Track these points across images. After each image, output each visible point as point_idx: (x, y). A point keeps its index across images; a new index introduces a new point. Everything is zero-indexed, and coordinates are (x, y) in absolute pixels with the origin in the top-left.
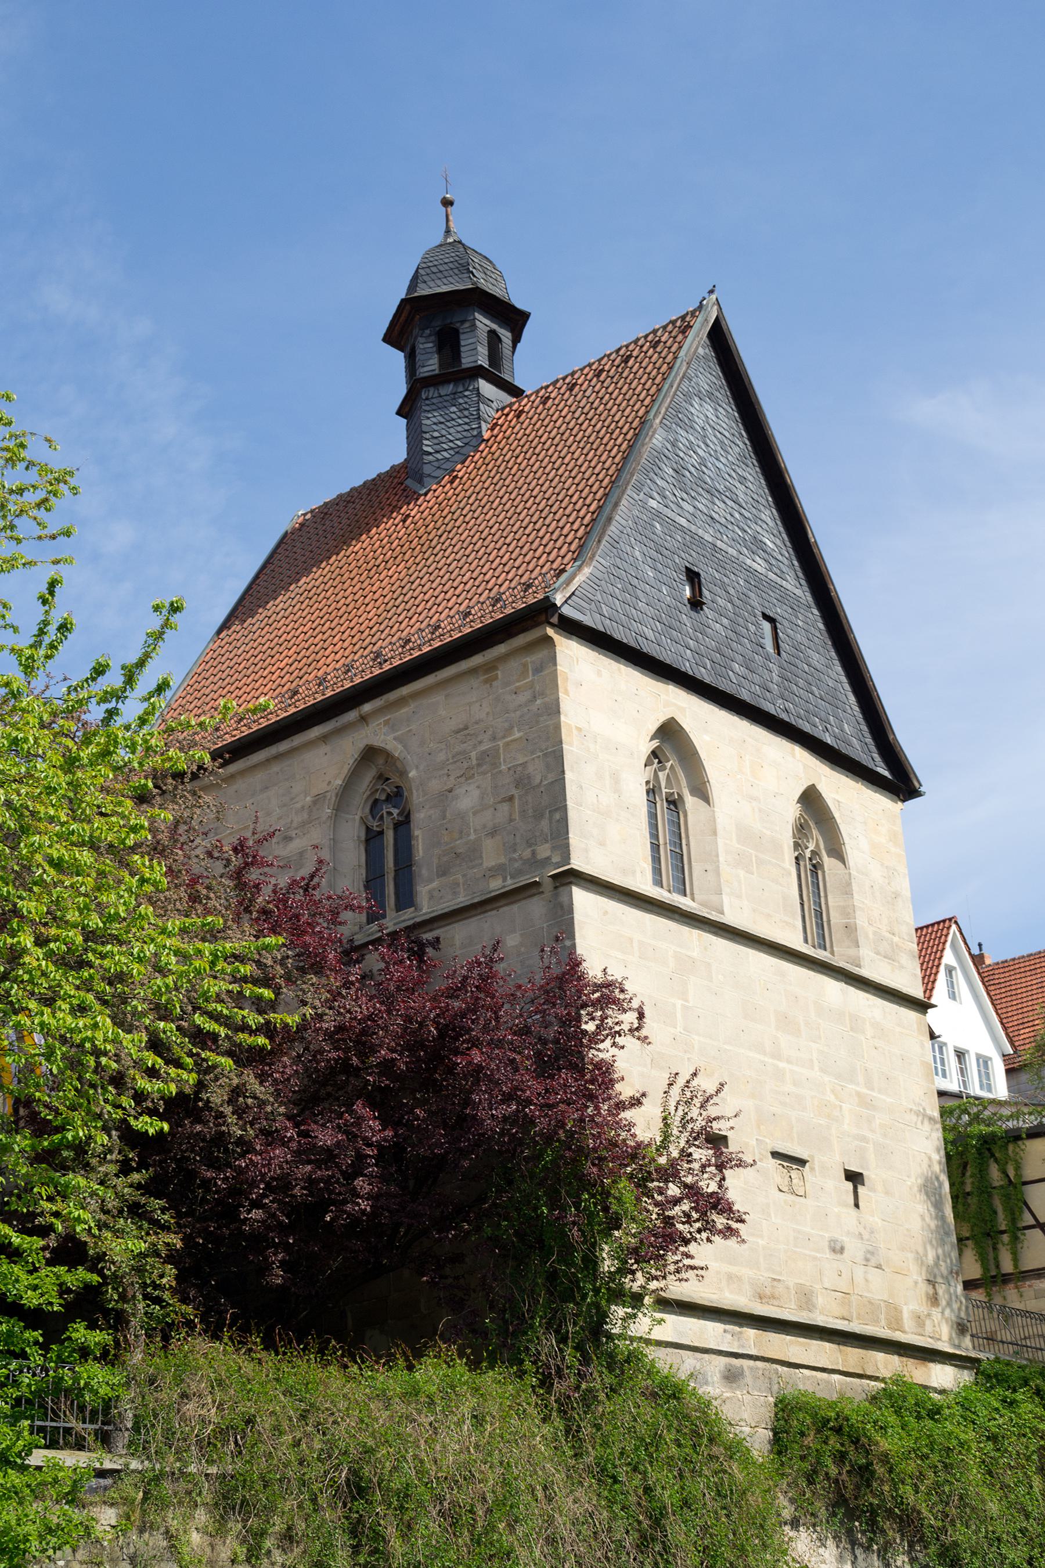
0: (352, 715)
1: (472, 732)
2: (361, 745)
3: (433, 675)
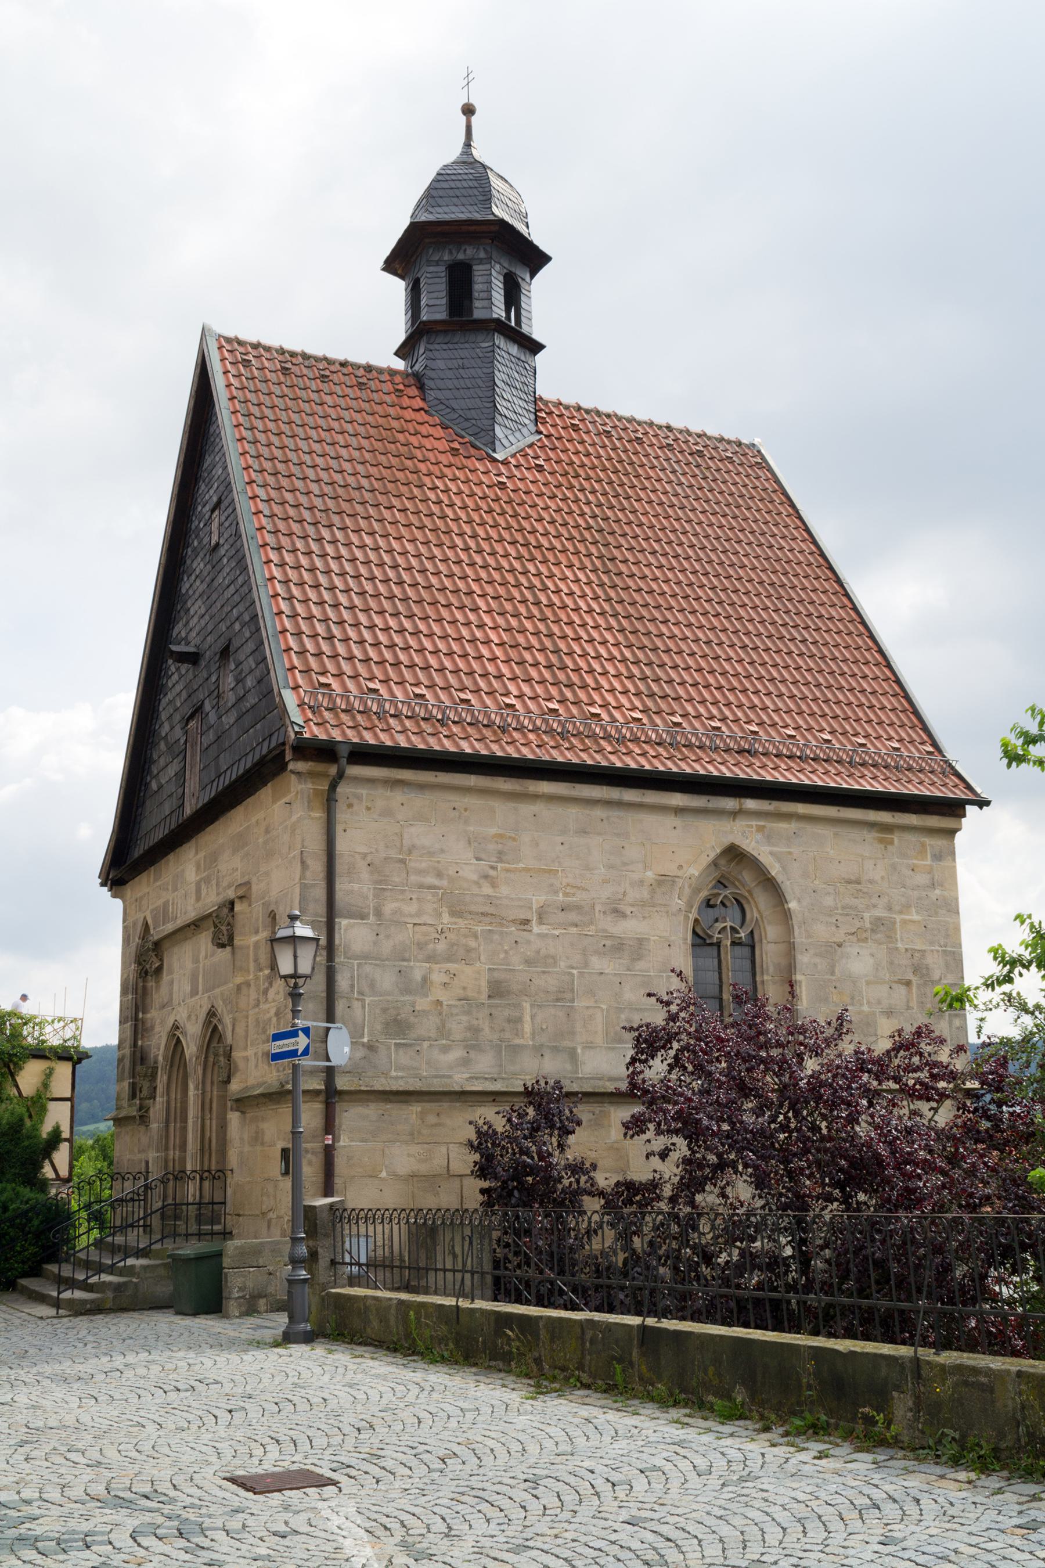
0: (730, 803)
1: (865, 890)
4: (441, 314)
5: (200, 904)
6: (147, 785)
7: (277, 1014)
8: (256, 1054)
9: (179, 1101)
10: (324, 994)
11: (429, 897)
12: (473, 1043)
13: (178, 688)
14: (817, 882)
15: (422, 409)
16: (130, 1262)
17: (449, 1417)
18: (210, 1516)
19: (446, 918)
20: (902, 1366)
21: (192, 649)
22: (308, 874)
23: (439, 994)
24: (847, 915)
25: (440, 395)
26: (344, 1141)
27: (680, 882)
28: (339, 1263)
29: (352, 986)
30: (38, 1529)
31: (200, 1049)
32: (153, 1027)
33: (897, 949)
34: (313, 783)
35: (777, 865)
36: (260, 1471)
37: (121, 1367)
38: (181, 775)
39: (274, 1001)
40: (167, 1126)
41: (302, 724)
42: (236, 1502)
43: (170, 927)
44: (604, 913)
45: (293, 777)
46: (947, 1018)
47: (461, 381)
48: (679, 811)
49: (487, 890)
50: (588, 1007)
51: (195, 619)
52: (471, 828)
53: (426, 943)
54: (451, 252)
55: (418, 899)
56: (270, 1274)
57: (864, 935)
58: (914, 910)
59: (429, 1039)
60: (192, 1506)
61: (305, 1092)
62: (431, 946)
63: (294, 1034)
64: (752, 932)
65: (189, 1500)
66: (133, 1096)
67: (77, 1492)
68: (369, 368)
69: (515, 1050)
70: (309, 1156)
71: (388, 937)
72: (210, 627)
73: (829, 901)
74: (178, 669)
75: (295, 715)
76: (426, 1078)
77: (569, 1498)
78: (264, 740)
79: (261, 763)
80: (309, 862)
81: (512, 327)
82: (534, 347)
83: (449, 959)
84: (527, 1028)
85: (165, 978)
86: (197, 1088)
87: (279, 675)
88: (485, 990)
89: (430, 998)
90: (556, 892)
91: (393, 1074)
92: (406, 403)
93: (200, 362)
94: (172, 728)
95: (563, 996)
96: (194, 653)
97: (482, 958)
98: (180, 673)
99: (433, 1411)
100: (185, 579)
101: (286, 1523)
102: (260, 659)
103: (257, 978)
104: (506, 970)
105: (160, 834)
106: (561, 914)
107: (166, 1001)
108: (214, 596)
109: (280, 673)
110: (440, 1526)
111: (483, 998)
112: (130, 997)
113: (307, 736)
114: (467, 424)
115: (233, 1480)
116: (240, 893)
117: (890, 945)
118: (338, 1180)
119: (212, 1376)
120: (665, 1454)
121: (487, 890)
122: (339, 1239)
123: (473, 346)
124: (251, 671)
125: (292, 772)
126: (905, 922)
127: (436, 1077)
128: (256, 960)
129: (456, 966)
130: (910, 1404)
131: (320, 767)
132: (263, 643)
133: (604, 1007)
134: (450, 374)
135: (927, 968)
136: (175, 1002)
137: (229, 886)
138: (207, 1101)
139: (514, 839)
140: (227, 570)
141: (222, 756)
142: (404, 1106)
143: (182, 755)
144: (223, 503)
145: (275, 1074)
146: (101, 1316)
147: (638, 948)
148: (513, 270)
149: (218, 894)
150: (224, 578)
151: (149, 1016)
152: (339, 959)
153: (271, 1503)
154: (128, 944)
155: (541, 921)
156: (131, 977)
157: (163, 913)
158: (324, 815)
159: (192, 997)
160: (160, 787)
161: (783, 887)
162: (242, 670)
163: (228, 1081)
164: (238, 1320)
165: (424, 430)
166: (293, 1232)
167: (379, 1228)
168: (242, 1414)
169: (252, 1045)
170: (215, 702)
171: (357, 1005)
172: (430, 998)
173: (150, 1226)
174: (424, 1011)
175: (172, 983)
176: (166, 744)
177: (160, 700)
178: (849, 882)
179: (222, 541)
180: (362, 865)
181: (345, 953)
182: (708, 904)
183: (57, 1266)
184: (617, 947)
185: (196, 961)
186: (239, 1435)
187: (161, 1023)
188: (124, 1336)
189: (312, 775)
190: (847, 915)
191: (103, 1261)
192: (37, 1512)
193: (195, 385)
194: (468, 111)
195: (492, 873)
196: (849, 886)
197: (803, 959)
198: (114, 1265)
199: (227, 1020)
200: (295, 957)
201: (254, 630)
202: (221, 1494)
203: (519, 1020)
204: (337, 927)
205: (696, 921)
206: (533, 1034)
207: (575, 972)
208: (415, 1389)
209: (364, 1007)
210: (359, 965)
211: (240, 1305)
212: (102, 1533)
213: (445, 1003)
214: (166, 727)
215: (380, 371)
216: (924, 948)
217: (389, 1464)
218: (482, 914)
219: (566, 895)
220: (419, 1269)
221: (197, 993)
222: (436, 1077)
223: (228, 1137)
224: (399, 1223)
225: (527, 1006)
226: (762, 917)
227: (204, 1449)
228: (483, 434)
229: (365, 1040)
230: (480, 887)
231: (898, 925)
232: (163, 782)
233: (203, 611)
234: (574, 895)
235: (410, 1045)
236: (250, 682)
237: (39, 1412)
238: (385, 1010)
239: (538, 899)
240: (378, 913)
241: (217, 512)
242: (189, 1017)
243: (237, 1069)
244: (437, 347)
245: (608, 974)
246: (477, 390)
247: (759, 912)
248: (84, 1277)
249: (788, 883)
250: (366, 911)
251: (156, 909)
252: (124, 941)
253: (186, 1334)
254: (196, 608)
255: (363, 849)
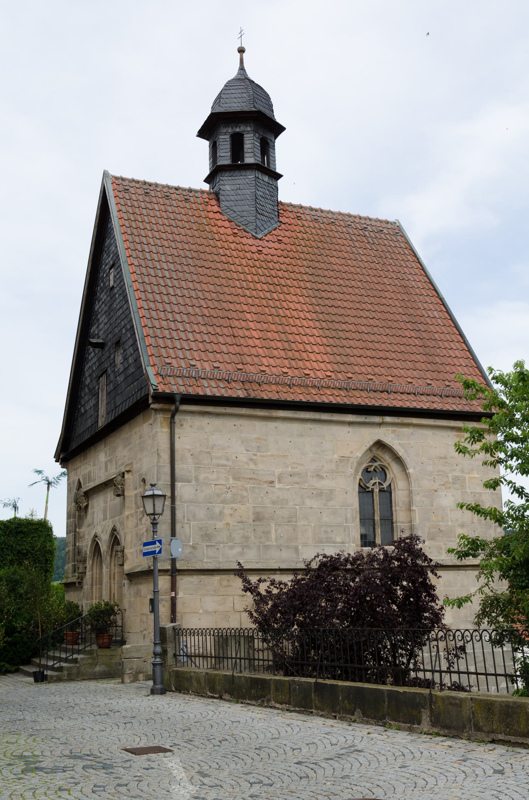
0: (377, 419)
1: (449, 462)
2: (376, 439)
3: (433, 420)
4: (227, 161)
5: (107, 473)
6: (79, 410)
7: (147, 531)
8: (136, 551)
9: (98, 574)
10: (170, 521)
11: (223, 471)
12: (245, 545)
13: (94, 360)
14: (424, 458)
15: (218, 212)
16: (75, 656)
17: (225, 725)
18: (116, 762)
19: (231, 481)
20: (425, 697)
21: (101, 341)
22: (161, 460)
23: (228, 520)
24: (439, 475)
25: (227, 204)
26: (180, 595)
27: (351, 460)
28: (178, 656)
29: (184, 517)
30: (43, 765)
31: (108, 548)
32: (84, 536)
33: (466, 492)
34: (163, 414)
35: (402, 450)
36: (138, 746)
37: (73, 705)
38: (96, 405)
39: (145, 524)
40: (92, 587)
41: (157, 385)
42: (127, 758)
43: (92, 485)
44: (312, 477)
45: (153, 411)
46: (493, 528)
47: (239, 196)
48: (350, 424)
49: (252, 466)
50: (304, 525)
51: (102, 325)
52: (244, 435)
53: (221, 494)
54: (232, 128)
55: (217, 472)
56: (145, 662)
57: (449, 485)
58: (475, 472)
59: (223, 543)
60: (108, 759)
61: (160, 571)
62: (224, 496)
63: (153, 543)
64: (390, 485)
65: (106, 757)
66: (74, 571)
67: (58, 753)
68: (190, 190)
69: (267, 547)
70: (163, 602)
71: (202, 491)
72: (110, 330)
73: (430, 468)
74: (94, 350)
75: (153, 380)
76: (222, 562)
77: (273, 755)
78: (138, 391)
79: (137, 403)
80: (161, 454)
81: (265, 168)
82: (279, 176)
83: (233, 502)
84: (273, 536)
85: (90, 510)
86: (107, 568)
87: (144, 360)
88: (252, 517)
89: (224, 522)
90: (287, 467)
91: (205, 560)
92: (209, 208)
93: (102, 190)
94: (91, 381)
95: (291, 520)
96: (102, 343)
97: (250, 501)
98: (95, 353)
99: (219, 722)
100: (97, 303)
101: (149, 765)
102: (136, 349)
103: (136, 512)
104: (262, 507)
105: (87, 436)
106: (290, 478)
107: (90, 522)
108: (112, 314)
109: (146, 358)
110: (215, 765)
111: (251, 521)
112: (72, 520)
113: (160, 391)
114: (241, 219)
115: (126, 750)
116: (127, 469)
117: (463, 491)
118: (178, 615)
119: (116, 709)
120: (319, 738)
121: (252, 466)
122: (177, 644)
123: (245, 177)
124: (131, 355)
125: (152, 408)
126: (471, 478)
127: (227, 562)
128: (136, 503)
129: (236, 505)
130: (429, 714)
131: (166, 406)
132: (137, 341)
133: (313, 525)
134: (233, 193)
135: (483, 502)
136: (95, 523)
137: (122, 465)
138: (112, 574)
139: (265, 440)
140: (118, 301)
141: (117, 397)
142: (211, 577)
143: (96, 396)
144: (116, 264)
145: (146, 561)
146: (61, 683)
147: (330, 494)
148: (265, 136)
149: (116, 469)
150: (117, 305)
151: (81, 530)
152: (178, 503)
153: (142, 758)
154: (71, 493)
155: (280, 481)
156: (72, 509)
157: (89, 477)
158: (169, 430)
159: (104, 521)
160: (86, 411)
161: (405, 461)
162: (127, 354)
163: (122, 565)
164: (129, 684)
165: (220, 223)
166: (155, 640)
167: (200, 638)
168: (131, 724)
169: (135, 546)
170: (113, 369)
171: (186, 526)
172: (224, 522)
173: (85, 638)
174: (220, 528)
175: (93, 513)
176: (89, 389)
177: (85, 366)
178: (441, 458)
179: (115, 286)
180: (188, 455)
181: (180, 500)
182: (366, 470)
183: (39, 659)
184: (319, 494)
185: (106, 502)
186: (129, 732)
187: (88, 534)
188: (74, 692)
189: (162, 410)
190: (439, 475)
191: (61, 656)
192: (41, 760)
193: (100, 202)
194: (241, 51)
195: (255, 457)
196: (441, 460)
197: (417, 498)
198: (67, 658)
199: (122, 533)
200: (154, 505)
201: (132, 334)
202: (121, 755)
203: (269, 532)
204: (176, 487)
205: (360, 479)
206: (276, 540)
207: (297, 507)
208: (211, 713)
209: (190, 527)
210: (188, 506)
211: (130, 677)
212: (70, 767)
213: (231, 524)
214: (88, 380)
215: (196, 191)
216: (481, 491)
217: (196, 744)
218: (250, 478)
219: (292, 468)
220: (219, 658)
221: (106, 519)
222: (227, 562)
223: (123, 593)
224: (206, 635)
225: (273, 525)
226: (395, 477)
227: (113, 738)
228: (250, 224)
229: (191, 544)
230: (248, 465)
231: (467, 480)
232: (87, 408)
233: (106, 321)
234: (296, 468)
235: (214, 546)
236: (131, 360)
237: (37, 724)
238: (201, 529)
239: (278, 471)
240: (197, 479)
241: (112, 270)
242: (103, 531)
243: (127, 559)
244: (226, 178)
245: (314, 508)
246: (247, 201)
247: (394, 474)
248: (52, 663)
249: (408, 459)
250: (190, 478)
251: (84, 475)
252: (68, 490)
253: (104, 691)
254: (103, 319)
255: (188, 447)
